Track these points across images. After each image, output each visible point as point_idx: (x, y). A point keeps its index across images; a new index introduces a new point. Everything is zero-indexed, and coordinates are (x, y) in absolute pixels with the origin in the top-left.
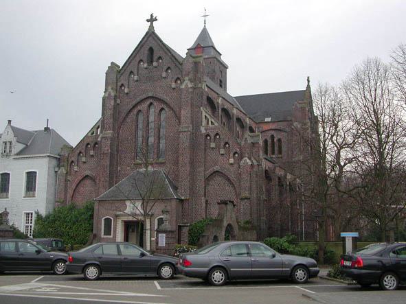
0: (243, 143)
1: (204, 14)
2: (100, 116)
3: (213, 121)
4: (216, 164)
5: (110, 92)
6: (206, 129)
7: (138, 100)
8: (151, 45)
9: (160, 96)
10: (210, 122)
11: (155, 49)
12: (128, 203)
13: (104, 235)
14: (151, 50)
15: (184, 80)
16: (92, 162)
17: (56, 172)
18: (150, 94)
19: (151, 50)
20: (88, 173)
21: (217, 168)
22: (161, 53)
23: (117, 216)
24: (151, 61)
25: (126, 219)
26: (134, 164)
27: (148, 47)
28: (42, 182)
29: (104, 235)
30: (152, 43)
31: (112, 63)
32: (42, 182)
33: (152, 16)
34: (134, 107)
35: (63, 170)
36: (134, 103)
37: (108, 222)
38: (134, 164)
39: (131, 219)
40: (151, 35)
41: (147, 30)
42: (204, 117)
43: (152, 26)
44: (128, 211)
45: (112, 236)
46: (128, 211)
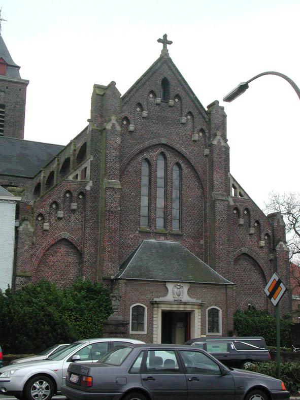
0: (276, 224)
3: (88, 172)
4: (243, 245)
7: (147, 144)
8: (165, 75)
9: (177, 147)
12: (170, 287)
13: (143, 330)
14: (165, 83)
16: (75, 219)
18: (164, 142)
19: (165, 83)
20: (66, 235)
21: (245, 250)
23: (153, 304)
24: (166, 98)
25: (167, 308)
29: (143, 330)
30: (168, 74)
31: (29, 81)
33: (165, 36)
34: (141, 152)
35: (28, 227)
36: (141, 146)
37: (138, 311)
39: (175, 308)
40: (165, 61)
41: (158, 57)
42: (84, 166)
43: (165, 52)
44: (169, 297)
45: (145, 332)
46: (169, 297)
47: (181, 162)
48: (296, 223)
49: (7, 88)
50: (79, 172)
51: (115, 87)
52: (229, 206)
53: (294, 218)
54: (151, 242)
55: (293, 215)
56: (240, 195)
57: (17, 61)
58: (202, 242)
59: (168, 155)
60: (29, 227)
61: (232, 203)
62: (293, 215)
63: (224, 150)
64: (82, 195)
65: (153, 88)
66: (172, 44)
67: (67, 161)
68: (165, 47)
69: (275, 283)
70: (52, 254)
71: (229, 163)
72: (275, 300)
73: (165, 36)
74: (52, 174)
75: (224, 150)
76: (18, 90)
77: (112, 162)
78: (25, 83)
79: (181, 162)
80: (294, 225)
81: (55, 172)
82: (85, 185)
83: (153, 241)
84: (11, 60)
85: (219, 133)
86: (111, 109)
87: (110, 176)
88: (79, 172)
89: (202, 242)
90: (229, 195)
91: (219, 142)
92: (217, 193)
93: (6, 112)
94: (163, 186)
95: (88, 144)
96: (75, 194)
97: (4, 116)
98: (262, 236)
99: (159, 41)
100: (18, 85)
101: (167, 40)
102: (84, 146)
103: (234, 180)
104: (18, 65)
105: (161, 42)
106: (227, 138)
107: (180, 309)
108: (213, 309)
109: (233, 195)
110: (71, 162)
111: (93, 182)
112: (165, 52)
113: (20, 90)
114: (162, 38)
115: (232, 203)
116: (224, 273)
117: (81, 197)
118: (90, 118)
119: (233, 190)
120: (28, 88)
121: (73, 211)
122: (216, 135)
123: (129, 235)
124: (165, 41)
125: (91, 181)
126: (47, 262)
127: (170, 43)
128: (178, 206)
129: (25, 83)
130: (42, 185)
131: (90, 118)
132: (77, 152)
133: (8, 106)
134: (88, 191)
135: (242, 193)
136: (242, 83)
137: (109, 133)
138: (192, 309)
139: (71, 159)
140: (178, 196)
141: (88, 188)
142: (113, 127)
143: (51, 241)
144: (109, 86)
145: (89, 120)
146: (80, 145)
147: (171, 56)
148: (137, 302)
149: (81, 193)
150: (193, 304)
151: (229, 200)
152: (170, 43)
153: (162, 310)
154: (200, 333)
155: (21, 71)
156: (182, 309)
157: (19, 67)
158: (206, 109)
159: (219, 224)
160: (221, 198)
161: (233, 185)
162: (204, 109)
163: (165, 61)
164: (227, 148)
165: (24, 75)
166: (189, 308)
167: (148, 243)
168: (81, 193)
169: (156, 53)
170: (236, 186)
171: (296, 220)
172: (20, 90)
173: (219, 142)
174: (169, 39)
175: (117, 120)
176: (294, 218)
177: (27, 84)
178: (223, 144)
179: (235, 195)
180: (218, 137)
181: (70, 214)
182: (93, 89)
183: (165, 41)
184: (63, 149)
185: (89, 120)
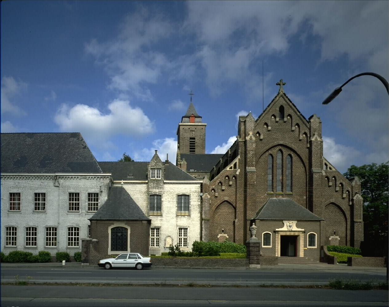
1: (192, 96)
2: (225, 153)
3: (237, 164)
5: (251, 137)
6: (326, 173)
10: (328, 169)
11: (286, 108)
13: (112, 250)
14: (282, 109)
15: (314, 135)
17: (201, 196)
18: (281, 142)
19: (282, 109)
20: (226, 198)
22: (291, 112)
26: (267, 194)
27: (279, 106)
28: (195, 202)
32: (195, 202)
34: (267, 150)
38: (267, 194)
46: (285, 228)
61: (324, 174)
75: (319, 143)
82: (236, 171)
91: (316, 139)
123: (261, 196)
141: (238, 173)
142: (251, 139)
166: (296, 234)
168: (234, 176)
173: (316, 139)
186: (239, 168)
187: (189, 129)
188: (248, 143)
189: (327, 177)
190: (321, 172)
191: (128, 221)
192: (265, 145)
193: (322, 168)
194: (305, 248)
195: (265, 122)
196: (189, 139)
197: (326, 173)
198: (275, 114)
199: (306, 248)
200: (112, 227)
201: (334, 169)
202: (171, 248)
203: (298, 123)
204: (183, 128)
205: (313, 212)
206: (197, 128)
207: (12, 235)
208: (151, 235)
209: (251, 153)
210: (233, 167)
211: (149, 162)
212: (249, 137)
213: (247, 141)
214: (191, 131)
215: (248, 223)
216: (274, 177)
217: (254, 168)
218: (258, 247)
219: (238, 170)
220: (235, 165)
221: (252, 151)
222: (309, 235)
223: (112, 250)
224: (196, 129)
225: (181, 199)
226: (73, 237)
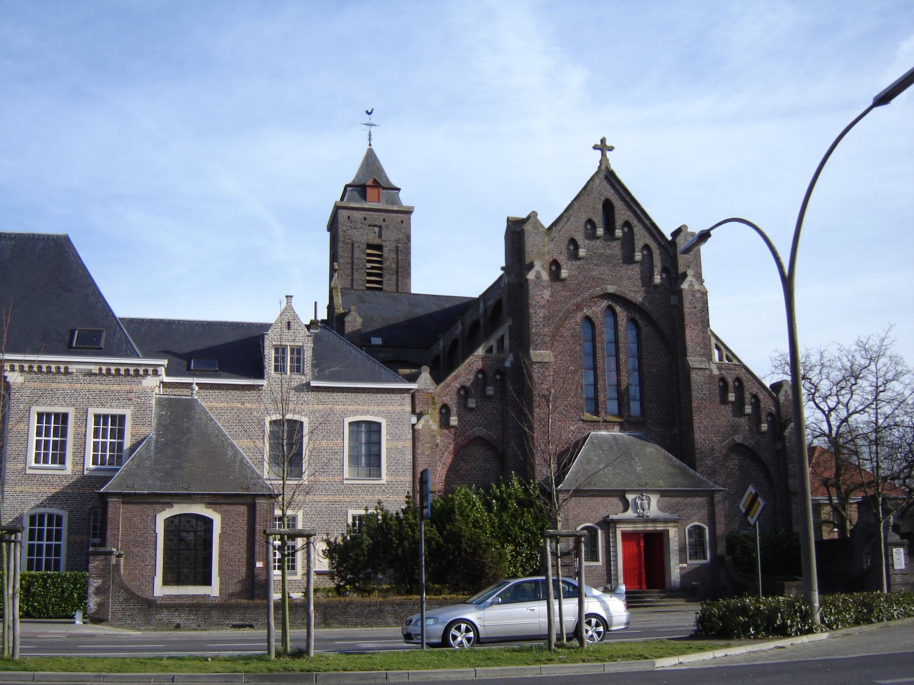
1: (373, 128)
3: (507, 342)
5: (538, 272)
6: (719, 369)
13: (166, 582)
18: (611, 289)
19: (608, 206)
25: (629, 528)
33: (603, 141)
43: (604, 160)
45: (160, 590)
47: (637, 317)
48: (815, 393)
49: (384, 220)
50: (493, 342)
51: (537, 219)
52: (711, 376)
53: (813, 384)
54: (601, 434)
55: (810, 379)
56: (728, 358)
57: (395, 181)
58: (675, 431)
59: (618, 309)
60: (431, 422)
61: (716, 372)
62: (810, 379)
63: (698, 295)
64: (500, 375)
65: (591, 216)
66: (614, 150)
67: (476, 324)
68: (603, 155)
69: (751, 496)
70: (463, 460)
71: (708, 313)
72: (752, 518)
73: (603, 141)
74: (455, 342)
75: (698, 295)
76: (400, 222)
77: (539, 325)
78: (408, 212)
79: (637, 317)
80: (813, 394)
81: (460, 341)
82: (504, 360)
83: (604, 433)
84: (387, 180)
85: (690, 272)
86: (532, 251)
87: (537, 345)
88: (493, 342)
89: (675, 431)
90: (711, 360)
91: (691, 285)
92: (693, 361)
93: (384, 255)
94: (614, 353)
95: (504, 301)
96: (490, 374)
97: (382, 267)
98: (763, 418)
99: (595, 148)
100: (400, 215)
101: (605, 145)
102: (499, 304)
103: (717, 338)
104: (397, 186)
105: (598, 149)
106: (703, 278)
107: (648, 529)
108: (695, 526)
109: (717, 360)
110: (482, 327)
111: (514, 355)
112: (604, 160)
113: (402, 222)
114: (599, 143)
115: (716, 372)
116: (710, 474)
117: (498, 377)
118: (504, 265)
119: (716, 352)
120: (413, 216)
121: (489, 398)
122: (685, 275)
123: (569, 427)
124: (603, 147)
125: (512, 355)
126: (458, 471)
127: (611, 149)
128: (637, 381)
129: (408, 212)
130: (441, 358)
131: (504, 265)
132: (489, 312)
133: (386, 246)
134: (507, 368)
135: (730, 356)
136: (702, 231)
137: (533, 284)
138: (665, 528)
139: (482, 322)
140: (637, 366)
141: (508, 364)
142: (538, 277)
143: (461, 441)
144: (529, 217)
145: (502, 269)
146: (491, 302)
147: (614, 167)
148: (585, 521)
149: (498, 372)
150: (666, 521)
151: (711, 368)
152: (611, 149)
153: (622, 531)
154: (678, 562)
155: (401, 195)
156: (651, 529)
157: (399, 189)
158: (670, 238)
159: (698, 403)
160: (698, 367)
161: (716, 344)
162: (666, 239)
163: (607, 176)
164: (705, 293)
165: (405, 199)
166: (660, 527)
167: (597, 437)
168: (498, 372)
169: (590, 165)
170: (721, 346)
171: (816, 387)
172: (402, 222)
173: (691, 285)
174: (609, 143)
175: (543, 266)
176: (813, 384)
177: (411, 212)
178: (697, 287)
179: (721, 359)
180: (689, 278)
181: (485, 401)
182: (506, 224)
183: (603, 147)
184: (467, 305)
185: (502, 269)
186: (510, 352)
187: (365, 219)
188: (531, 287)
189: (723, 379)
190: (708, 367)
191: (213, 500)
192: (574, 295)
193: (710, 358)
194: (681, 565)
195: (570, 238)
196: (365, 246)
197: (719, 371)
198: (592, 218)
199: (685, 565)
200: (168, 513)
201: (735, 362)
202: (23, 600)
203: (649, 244)
204: (349, 218)
205: (695, 470)
206: (386, 220)
207: (43, 545)
208: (65, 528)
209: (541, 313)
210: (495, 348)
211: (271, 325)
212: (535, 273)
213: (529, 282)
214: (369, 226)
215: (378, 339)
216: (600, 377)
217: (548, 352)
218: (567, 565)
219: (508, 356)
220: (501, 341)
221: (543, 307)
222: (705, 529)
223: (166, 582)
224: (384, 220)
225: (359, 432)
226: (45, 543)
